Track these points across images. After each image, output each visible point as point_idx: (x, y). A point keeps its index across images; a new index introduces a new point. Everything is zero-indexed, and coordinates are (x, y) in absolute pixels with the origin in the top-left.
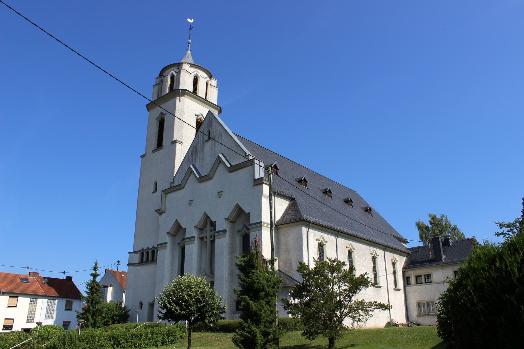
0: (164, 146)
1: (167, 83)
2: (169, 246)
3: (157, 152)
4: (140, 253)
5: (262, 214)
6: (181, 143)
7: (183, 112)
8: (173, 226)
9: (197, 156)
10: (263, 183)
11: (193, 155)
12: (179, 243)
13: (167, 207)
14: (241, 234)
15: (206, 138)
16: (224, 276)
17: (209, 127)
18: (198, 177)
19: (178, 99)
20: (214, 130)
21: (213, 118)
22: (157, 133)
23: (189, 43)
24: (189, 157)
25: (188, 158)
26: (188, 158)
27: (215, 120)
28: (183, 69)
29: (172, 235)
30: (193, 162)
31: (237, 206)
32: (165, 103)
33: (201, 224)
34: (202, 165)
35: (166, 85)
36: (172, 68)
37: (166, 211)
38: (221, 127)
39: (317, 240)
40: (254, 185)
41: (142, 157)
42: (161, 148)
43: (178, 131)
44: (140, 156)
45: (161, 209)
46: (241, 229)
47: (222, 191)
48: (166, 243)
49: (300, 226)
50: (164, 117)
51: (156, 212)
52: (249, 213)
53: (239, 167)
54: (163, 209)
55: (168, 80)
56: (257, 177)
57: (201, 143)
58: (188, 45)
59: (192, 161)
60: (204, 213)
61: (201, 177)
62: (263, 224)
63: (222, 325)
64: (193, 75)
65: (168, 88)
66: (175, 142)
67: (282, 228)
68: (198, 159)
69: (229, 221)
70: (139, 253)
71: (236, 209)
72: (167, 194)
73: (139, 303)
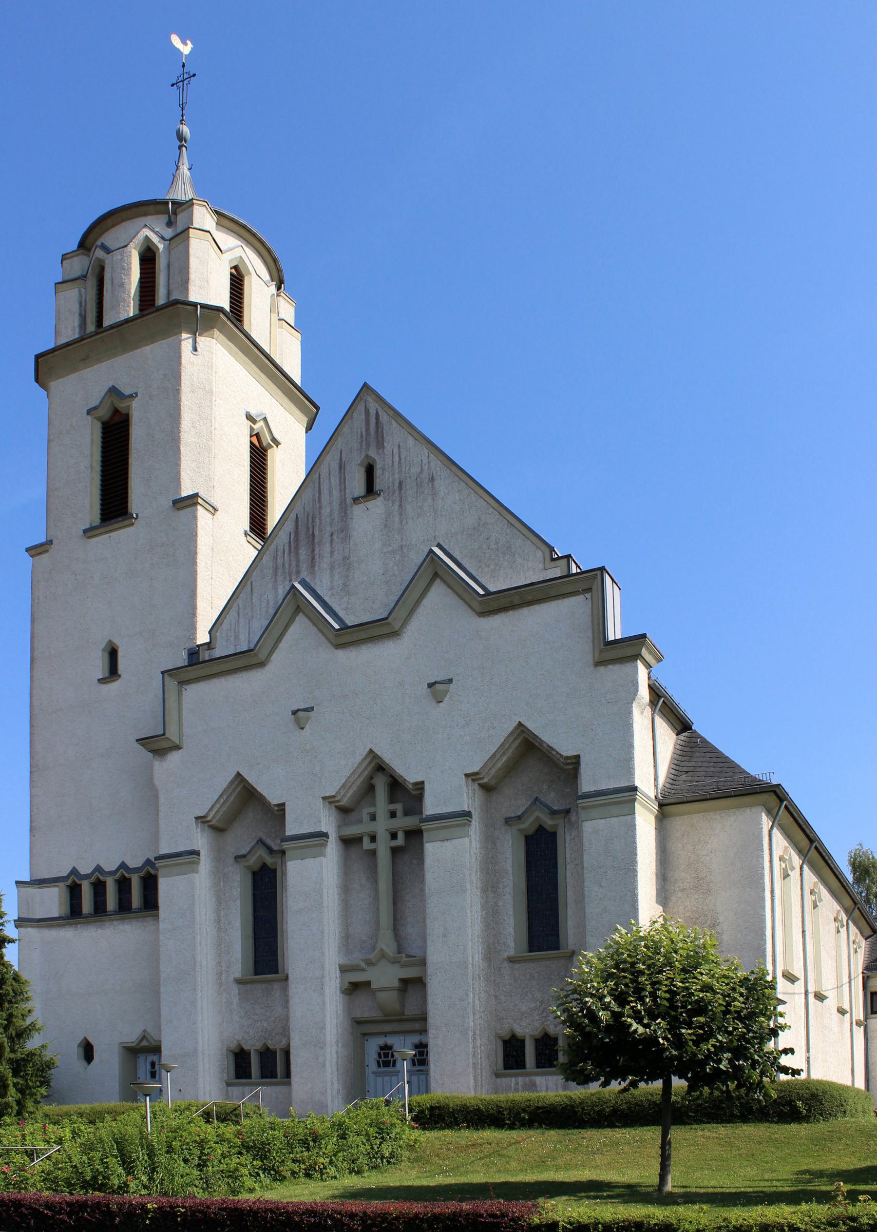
0: (137, 515)
1: (129, 275)
2: (205, 863)
3: (107, 536)
4: (62, 885)
5: (636, 762)
6: (211, 509)
7: (211, 392)
8: (222, 794)
9: (316, 552)
10: (638, 656)
11: (297, 548)
12: (244, 856)
13: (186, 730)
14: (520, 830)
15: (358, 485)
16: (470, 959)
17: (368, 446)
18: (337, 627)
19: (186, 341)
20: (396, 458)
21: (384, 418)
22: (98, 467)
23: (180, 137)
24: (280, 554)
25: (276, 557)
26: (276, 557)
27: (394, 424)
28: (195, 225)
29: (213, 828)
30: (298, 572)
31: (517, 732)
32: (125, 351)
33: (351, 792)
34: (345, 585)
35: (122, 285)
36: (148, 220)
37: (187, 743)
38: (426, 452)
39: (780, 860)
40: (599, 663)
41: (36, 551)
42: (127, 522)
43: (195, 464)
44: (27, 550)
45: (164, 734)
47: (450, 681)
49: (754, 810)
50: (129, 407)
52: (578, 757)
53: (530, 598)
54: (172, 734)
55: (129, 264)
56: (614, 632)
57: (336, 505)
58: (180, 147)
59: (294, 569)
60: (234, 774)
61: (345, 627)
62: (639, 796)
63: (545, 1107)
64: (230, 261)
65: (132, 295)
66: (193, 500)
67: (683, 814)
68: (324, 563)
69: (480, 785)
70: (61, 884)
71: (515, 739)
72: (182, 683)
73: (79, 1045)
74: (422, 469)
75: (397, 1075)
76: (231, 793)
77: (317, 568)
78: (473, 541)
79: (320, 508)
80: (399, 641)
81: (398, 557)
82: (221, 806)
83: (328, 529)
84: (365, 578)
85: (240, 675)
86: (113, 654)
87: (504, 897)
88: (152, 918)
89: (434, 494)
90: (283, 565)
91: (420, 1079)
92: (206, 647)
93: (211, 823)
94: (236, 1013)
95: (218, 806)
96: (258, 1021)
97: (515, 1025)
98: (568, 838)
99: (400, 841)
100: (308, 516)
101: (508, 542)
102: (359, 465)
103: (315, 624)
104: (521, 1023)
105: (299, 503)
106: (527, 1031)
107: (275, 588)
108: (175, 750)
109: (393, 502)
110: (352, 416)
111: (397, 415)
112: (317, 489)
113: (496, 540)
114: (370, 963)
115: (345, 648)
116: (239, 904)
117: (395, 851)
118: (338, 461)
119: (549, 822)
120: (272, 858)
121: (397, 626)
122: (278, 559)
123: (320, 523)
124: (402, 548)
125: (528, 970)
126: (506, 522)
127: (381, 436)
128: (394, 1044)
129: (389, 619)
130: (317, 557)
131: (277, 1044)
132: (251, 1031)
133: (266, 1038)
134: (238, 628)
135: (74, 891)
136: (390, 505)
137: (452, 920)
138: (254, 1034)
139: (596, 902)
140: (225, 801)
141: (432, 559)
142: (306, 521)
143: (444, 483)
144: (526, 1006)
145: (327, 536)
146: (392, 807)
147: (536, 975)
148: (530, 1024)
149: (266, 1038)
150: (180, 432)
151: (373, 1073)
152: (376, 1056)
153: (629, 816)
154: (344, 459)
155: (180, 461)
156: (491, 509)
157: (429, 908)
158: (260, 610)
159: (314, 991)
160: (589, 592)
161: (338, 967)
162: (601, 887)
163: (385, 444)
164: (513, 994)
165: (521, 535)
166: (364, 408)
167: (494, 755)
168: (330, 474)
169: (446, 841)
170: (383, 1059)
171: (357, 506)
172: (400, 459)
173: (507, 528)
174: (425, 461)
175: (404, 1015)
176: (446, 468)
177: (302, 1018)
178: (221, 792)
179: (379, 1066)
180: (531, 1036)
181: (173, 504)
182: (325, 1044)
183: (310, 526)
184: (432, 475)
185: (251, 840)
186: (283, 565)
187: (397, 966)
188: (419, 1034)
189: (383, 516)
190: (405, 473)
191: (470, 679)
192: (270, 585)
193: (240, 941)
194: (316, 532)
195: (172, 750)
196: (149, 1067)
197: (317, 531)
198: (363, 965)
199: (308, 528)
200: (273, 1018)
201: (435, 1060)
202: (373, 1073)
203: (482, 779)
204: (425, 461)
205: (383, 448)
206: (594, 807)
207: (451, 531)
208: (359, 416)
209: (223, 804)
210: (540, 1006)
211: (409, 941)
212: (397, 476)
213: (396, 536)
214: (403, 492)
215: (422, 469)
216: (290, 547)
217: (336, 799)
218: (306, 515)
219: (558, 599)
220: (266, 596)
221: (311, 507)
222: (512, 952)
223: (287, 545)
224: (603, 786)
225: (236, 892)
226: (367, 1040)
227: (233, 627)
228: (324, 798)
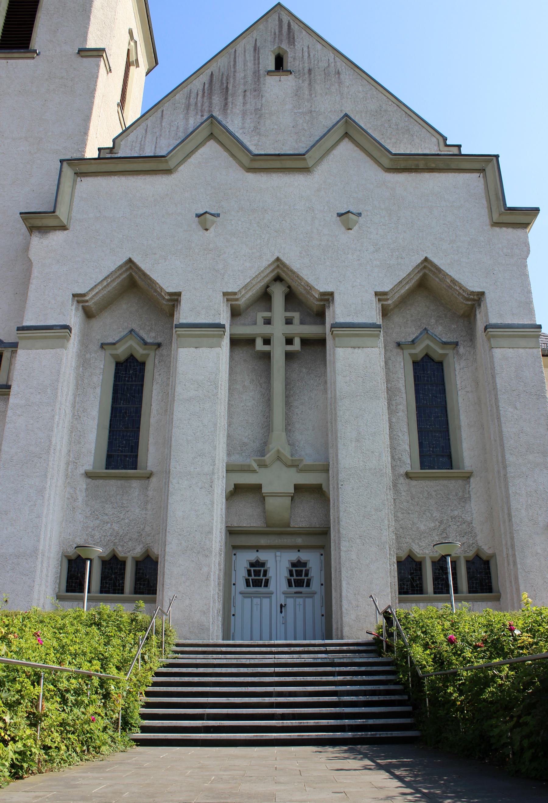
17: (281, 41)
20: (306, 54)
21: (295, 27)
24: (193, 95)
27: (304, 33)
33: (250, 294)
34: (256, 128)
38: (331, 54)
40: (495, 224)
46: (117, 339)
47: (218, 215)
48: (67, 327)
51: (24, 220)
53: (433, 166)
54: (62, 213)
57: (250, 73)
74: (329, 65)
75: (270, 597)
76: (115, 279)
77: (229, 111)
78: (376, 120)
79: (235, 72)
80: (309, 177)
81: (307, 118)
82: (102, 289)
83: (242, 87)
84: (276, 127)
85: (144, 177)
87: (397, 414)
89: (340, 83)
90: (196, 104)
91: (297, 603)
92: (108, 151)
93: (87, 304)
94: (80, 511)
95: (100, 287)
96: (107, 523)
97: (414, 545)
98: (457, 367)
99: (297, 346)
100: (222, 75)
101: (407, 126)
102: (272, 51)
104: (420, 543)
105: (215, 65)
106: (427, 552)
107: (187, 119)
108: (59, 230)
109: (303, 81)
110: (267, 21)
111: (306, 27)
112: (232, 60)
113: (396, 123)
114: (263, 465)
115: (256, 172)
116: (99, 392)
117: (289, 356)
118: (253, 45)
120: (144, 349)
121: (310, 163)
122: (191, 99)
123: (234, 82)
124: (311, 112)
125: (426, 488)
126: (404, 113)
127: (292, 37)
128: (267, 560)
129: (306, 156)
130: (230, 105)
131: (129, 552)
132: (97, 534)
133: (115, 544)
134: (144, 142)
136: (301, 82)
137: (366, 425)
138: (100, 538)
139: (513, 423)
140: (108, 285)
141: (346, 122)
142: (220, 78)
143: (347, 76)
144: (424, 525)
145: (240, 91)
146: (289, 314)
147: (434, 494)
148: (429, 545)
149: (115, 544)
150: (91, 7)
151: (241, 593)
152: (244, 574)
153: (534, 349)
154: (258, 45)
155: (89, 25)
156: (390, 103)
157: (340, 410)
158: (169, 132)
159: (201, 488)
160: (478, 173)
161: (225, 465)
162: (516, 408)
163: (296, 43)
164: (410, 512)
165: (417, 124)
166: (277, 17)
167: (400, 282)
168: (245, 52)
169: (357, 349)
170: (253, 577)
171: (270, 77)
172: (309, 55)
173: (405, 117)
174: (332, 60)
175: (289, 527)
176: (350, 68)
177: (183, 519)
178: (108, 274)
179: (248, 585)
180: (431, 558)
181: (79, 51)
182: (211, 552)
183: (224, 82)
184: (338, 70)
185: (121, 329)
186: (196, 104)
187: (293, 470)
188: (297, 551)
189: (294, 88)
190: (314, 64)
191: (378, 216)
192: (182, 116)
193: (96, 431)
194: (230, 87)
195: (56, 230)
197: (231, 86)
198: (255, 466)
199: (222, 83)
200: (127, 521)
201: (347, 577)
202: (241, 593)
203: (387, 300)
204: (332, 60)
205: (294, 46)
206: (503, 336)
207: (356, 109)
209: (105, 287)
210: (439, 526)
211: (297, 448)
212: (306, 65)
213: (306, 104)
214: (312, 76)
215: (329, 65)
217: (236, 297)
218: (221, 74)
219: (455, 172)
220: (176, 123)
221: (226, 69)
222: (408, 469)
223: (201, 91)
224: (508, 321)
225: (97, 379)
226: (235, 555)
227: (139, 140)
228: (225, 294)
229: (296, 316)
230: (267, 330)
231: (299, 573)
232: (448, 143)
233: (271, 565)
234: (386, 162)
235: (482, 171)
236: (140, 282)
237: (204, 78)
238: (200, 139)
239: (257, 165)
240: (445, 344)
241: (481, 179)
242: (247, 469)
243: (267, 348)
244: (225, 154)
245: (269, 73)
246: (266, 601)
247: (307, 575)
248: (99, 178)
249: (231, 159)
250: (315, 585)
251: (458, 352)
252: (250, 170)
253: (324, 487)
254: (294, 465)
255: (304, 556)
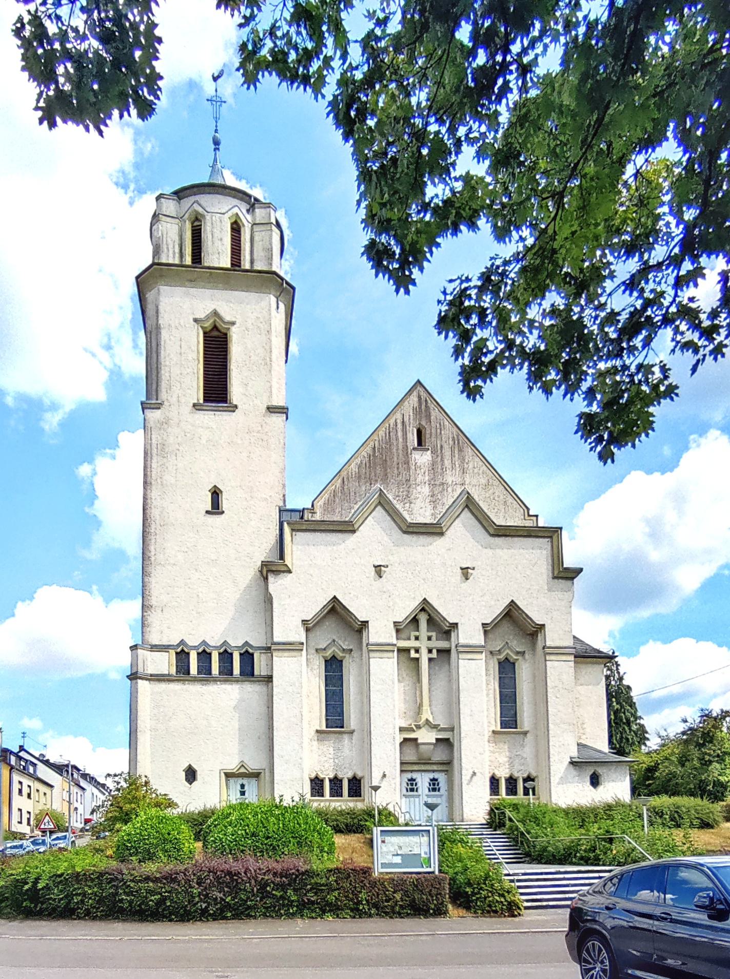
14: (498, 659)
86: (216, 494)
88: (200, 683)
99: (434, 654)
103: (390, 515)
119: (340, 654)
135: (182, 656)
146: (430, 634)
152: (419, 785)
179: (429, 791)
196: (239, 787)
208: (414, 399)
216: (370, 463)
229: (434, 634)
230: (416, 644)
231: (434, 784)
232: (531, 513)
233: (419, 780)
234: (492, 531)
235: (551, 537)
236: (339, 610)
237: (369, 449)
238: (372, 507)
239: (411, 530)
240: (518, 653)
241: (550, 543)
242: (410, 730)
243: (417, 656)
244: (389, 518)
245: (414, 449)
246: (417, 800)
247: (438, 785)
248: (307, 533)
249: (392, 523)
250: (443, 791)
251: (524, 659)
252: (405, 532)
253: (451, 740)
254: (435, 727)
255: (436, 775)
